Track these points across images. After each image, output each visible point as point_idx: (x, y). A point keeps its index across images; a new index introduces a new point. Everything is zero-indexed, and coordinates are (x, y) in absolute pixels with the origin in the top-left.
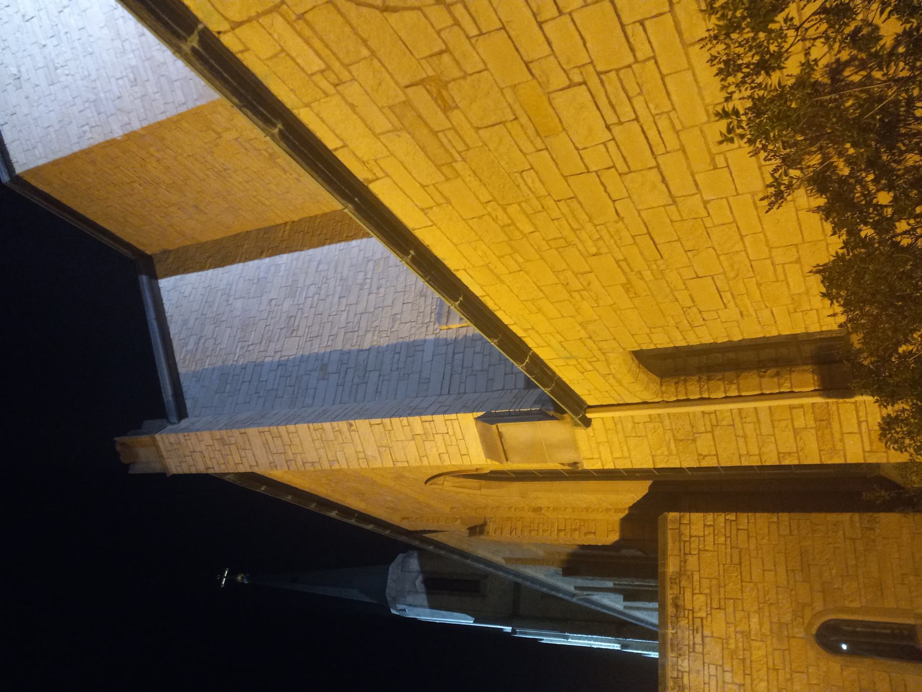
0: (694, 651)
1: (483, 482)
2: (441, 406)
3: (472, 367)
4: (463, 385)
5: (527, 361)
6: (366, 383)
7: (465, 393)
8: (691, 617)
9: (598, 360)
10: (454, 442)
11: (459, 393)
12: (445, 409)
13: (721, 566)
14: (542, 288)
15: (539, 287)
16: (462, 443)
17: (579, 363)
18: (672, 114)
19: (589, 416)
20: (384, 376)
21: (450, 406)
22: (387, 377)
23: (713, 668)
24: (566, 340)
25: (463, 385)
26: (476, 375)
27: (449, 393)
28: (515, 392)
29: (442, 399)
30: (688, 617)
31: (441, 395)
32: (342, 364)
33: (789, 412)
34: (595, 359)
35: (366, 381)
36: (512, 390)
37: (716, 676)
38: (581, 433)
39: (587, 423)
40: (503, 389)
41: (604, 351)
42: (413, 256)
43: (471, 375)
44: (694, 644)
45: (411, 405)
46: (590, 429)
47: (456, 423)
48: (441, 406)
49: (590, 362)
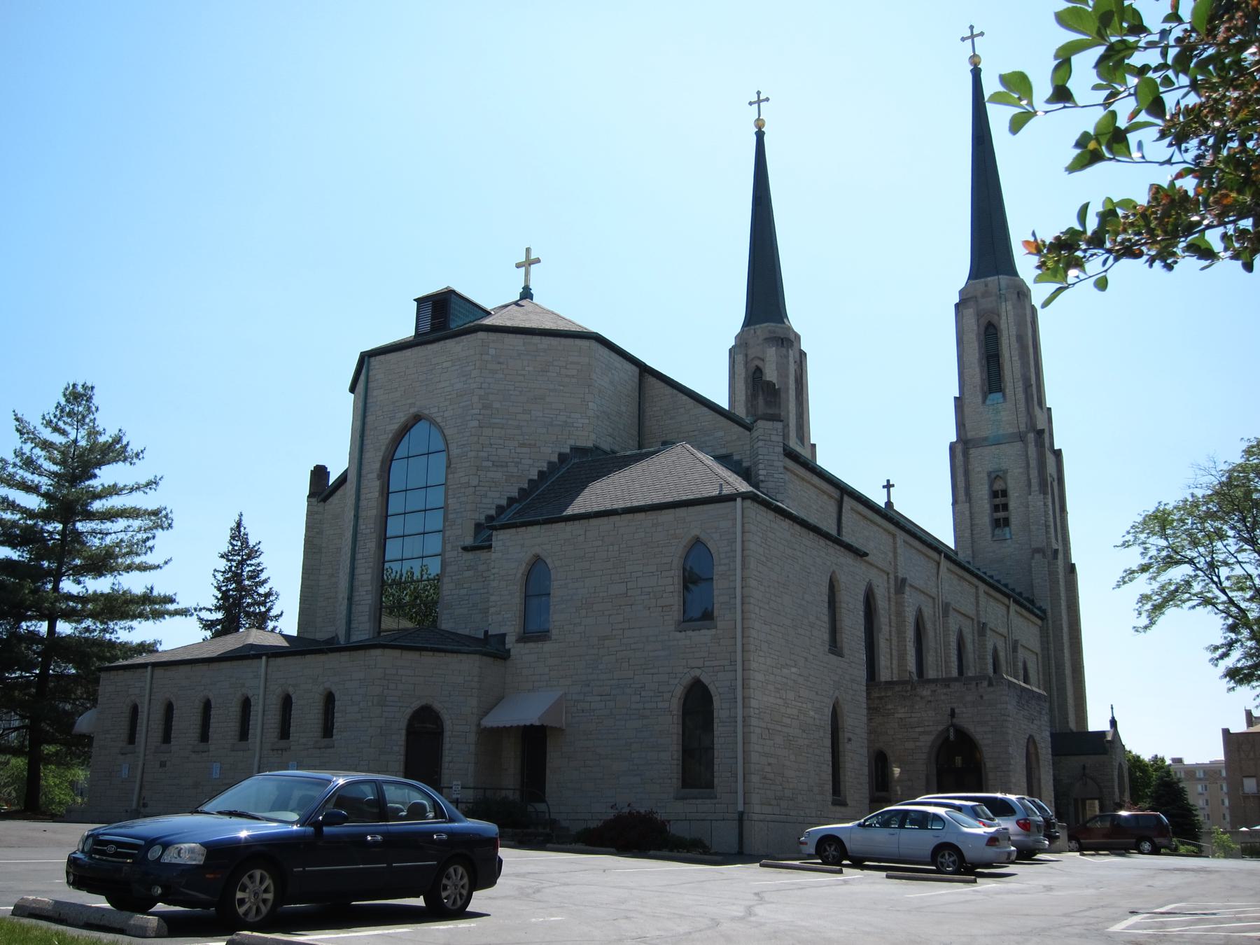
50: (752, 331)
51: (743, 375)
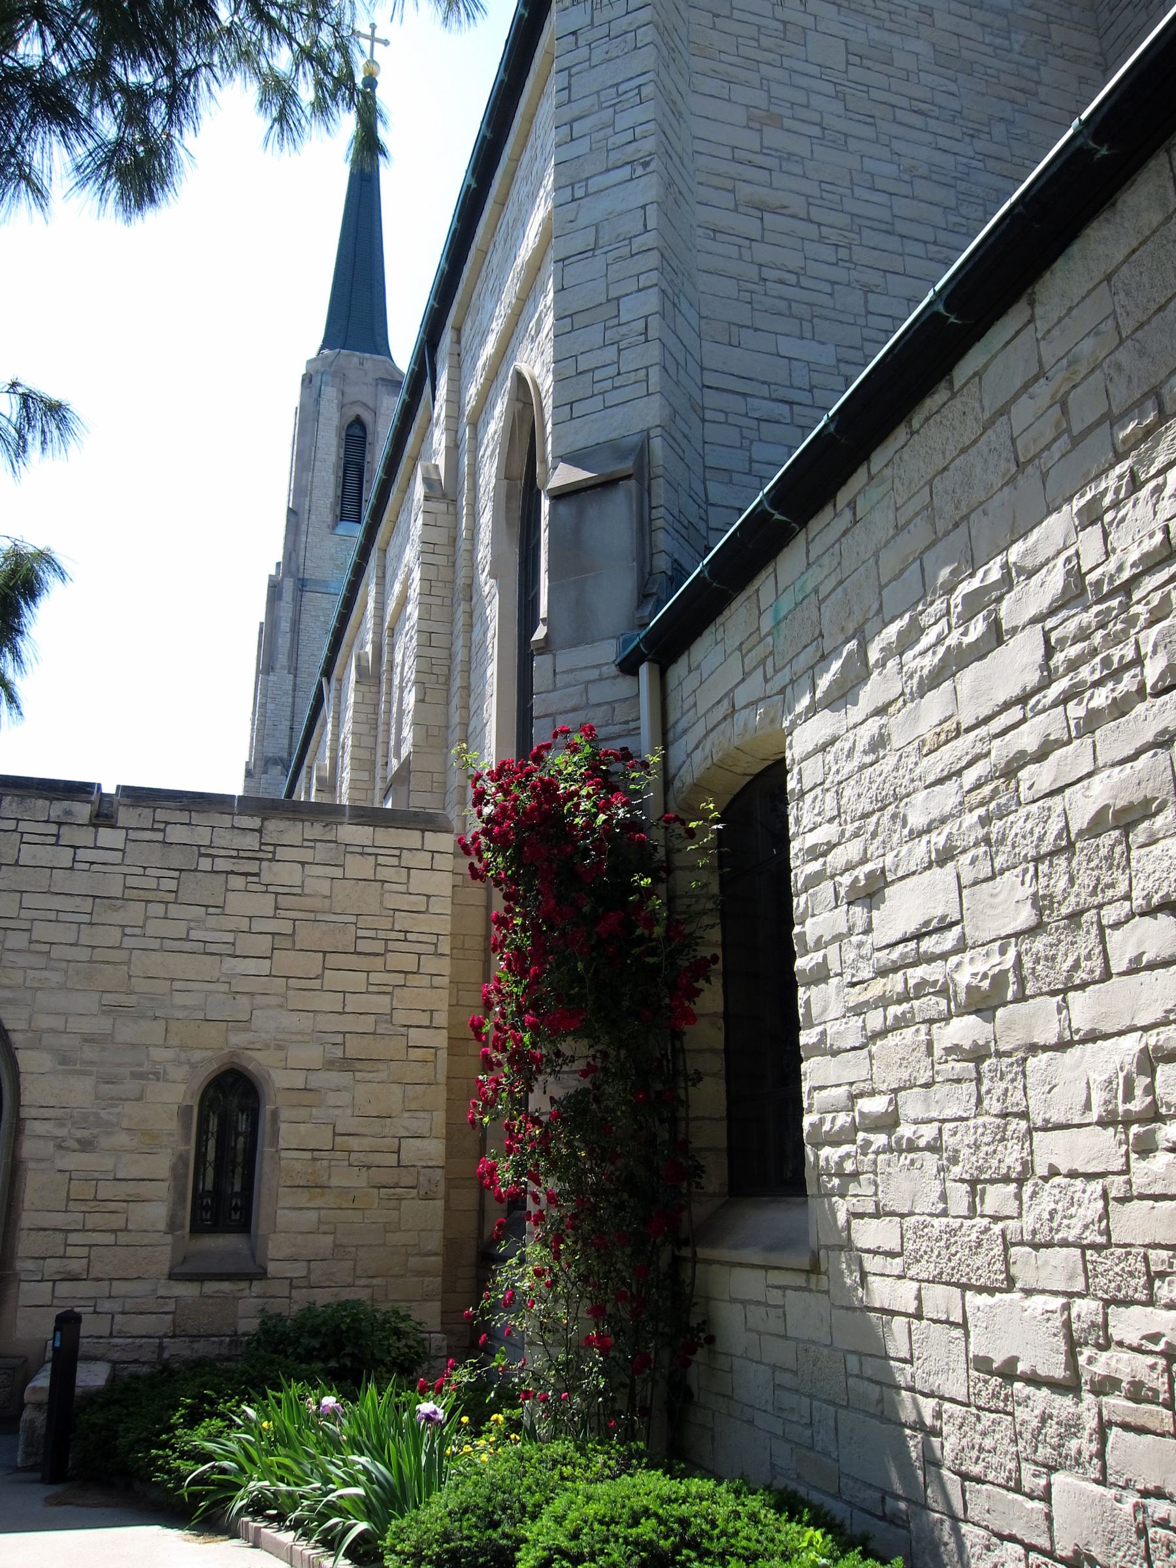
0: (201, 855)
1: (520, 484)
2: (678, 364)
3: (760, 440)
4: (721, 417)
5: (778, 516)
6: (736, 210)
7: (703, 420)
8: (261, 855)
9: (766, 680)
10: (598, 388)
11: (703, 408)
12: (672, 371)
13: (353, 919)
14: (963, 527)
15: (966, 517)
16: (597, 402)
17: (762, 640)
18: (346, 1163)
19: (644, 669)
20: (750, 248)
21: (677, 383)
22: (746, 254)
23: (172, 885)
24: (821, 602)
25: (721, 417)
26: (741, 447)
27: (704, 386)
28: (702, 526)
29: (693, 368)
30: (261, 850)
31: (702, 369)
32: (780, 158)
33: (967, 1177)
34: (770, 671)
35: (742, 209)
36: (707, 522)
37: (158, 889)
38: (607, 652)
39: (629, 667)
40: (707, 501)
41: (789, 689)
42: (1091, 152)
43: (743, 437)
44: (213, 857)
45: (682, 298)
46: (613, 670)
47: (641, 390)
48: (678, 364)
49: (763, 662)
50: (356, 360)
51: (335, 422)
